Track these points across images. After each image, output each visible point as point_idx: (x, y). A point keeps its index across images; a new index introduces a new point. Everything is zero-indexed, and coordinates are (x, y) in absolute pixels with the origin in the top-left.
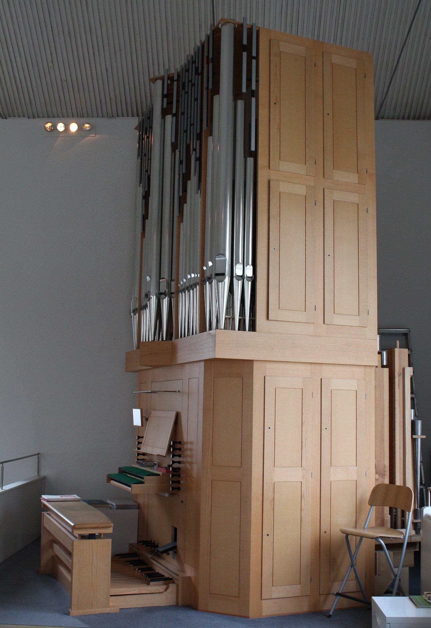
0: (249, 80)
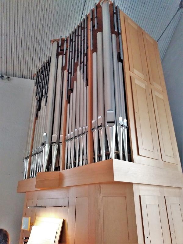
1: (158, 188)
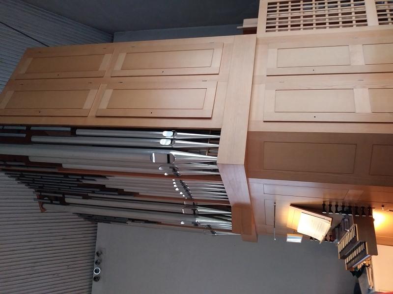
0: (19, 131)
1: (256, 86)
